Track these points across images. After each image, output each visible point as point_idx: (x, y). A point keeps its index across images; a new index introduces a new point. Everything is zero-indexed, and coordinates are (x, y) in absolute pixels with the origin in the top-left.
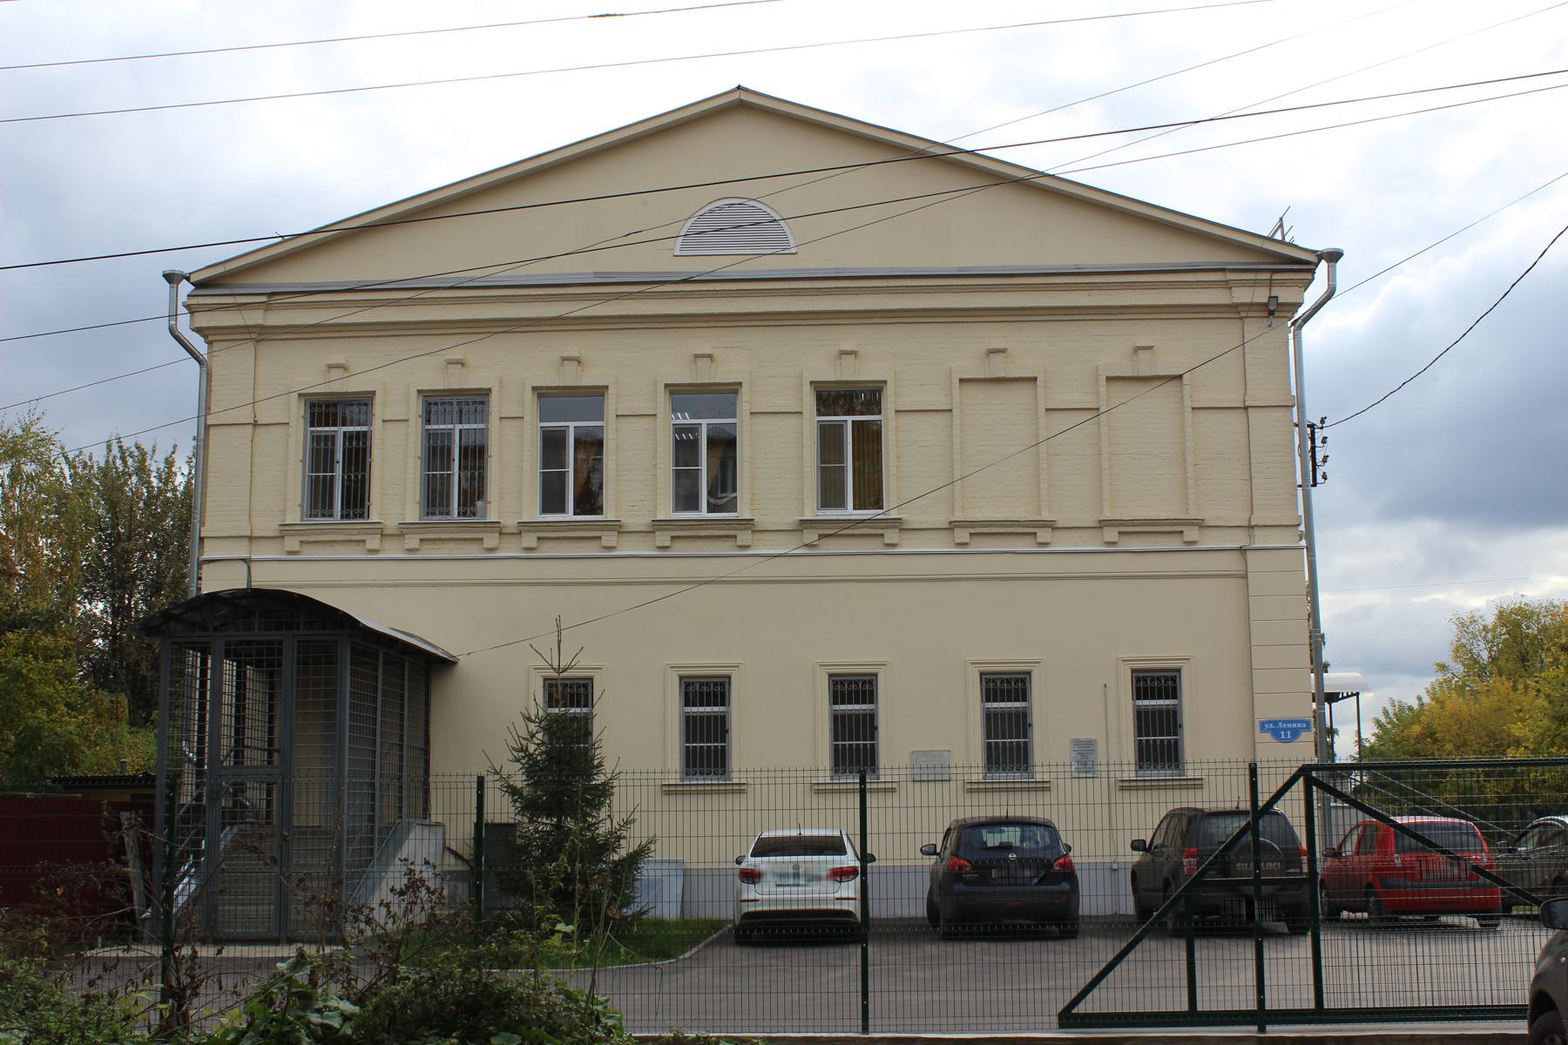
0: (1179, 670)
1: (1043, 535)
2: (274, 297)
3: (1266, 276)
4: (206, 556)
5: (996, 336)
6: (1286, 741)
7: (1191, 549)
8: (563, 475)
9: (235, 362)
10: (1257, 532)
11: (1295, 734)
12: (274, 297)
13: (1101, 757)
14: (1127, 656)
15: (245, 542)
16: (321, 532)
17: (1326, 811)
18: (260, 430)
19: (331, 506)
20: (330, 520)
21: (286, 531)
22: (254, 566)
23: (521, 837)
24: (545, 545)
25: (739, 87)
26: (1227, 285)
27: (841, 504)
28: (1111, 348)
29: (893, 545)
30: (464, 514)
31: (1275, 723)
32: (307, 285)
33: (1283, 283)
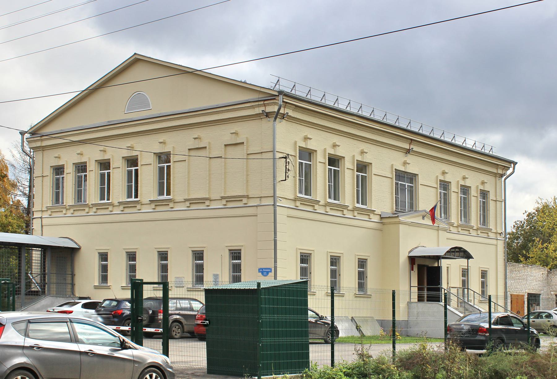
0: (241, 250)
1: (207, 203)
2: (50, 136)
3: (262, 103)
4: (34, 217)
5: (197, 132)
6: (265, 276)
7: (246, 206)
8: (164, 182)
9: (38, 156)
10: (263, 199)
11: (268, 273)
12: (50, 136)
13: (220, 280)
14: (124, 247)
15: (41, 212)
16: (56, 209)
17: (497, 308)
18: (44, 178)
19: (81, 199)
20: (58, 205)
21: (48, 208)
22: (43, 219)
23: (14, 299)
24: (99, 211)
25: (135, 54)
26: (253, 107)
27: (131, 197)
28: (224, 134)
29: (140, 210)
30: (78, 202)
31: (262, 269)
32: (57, 131)
33: (269, 105)
